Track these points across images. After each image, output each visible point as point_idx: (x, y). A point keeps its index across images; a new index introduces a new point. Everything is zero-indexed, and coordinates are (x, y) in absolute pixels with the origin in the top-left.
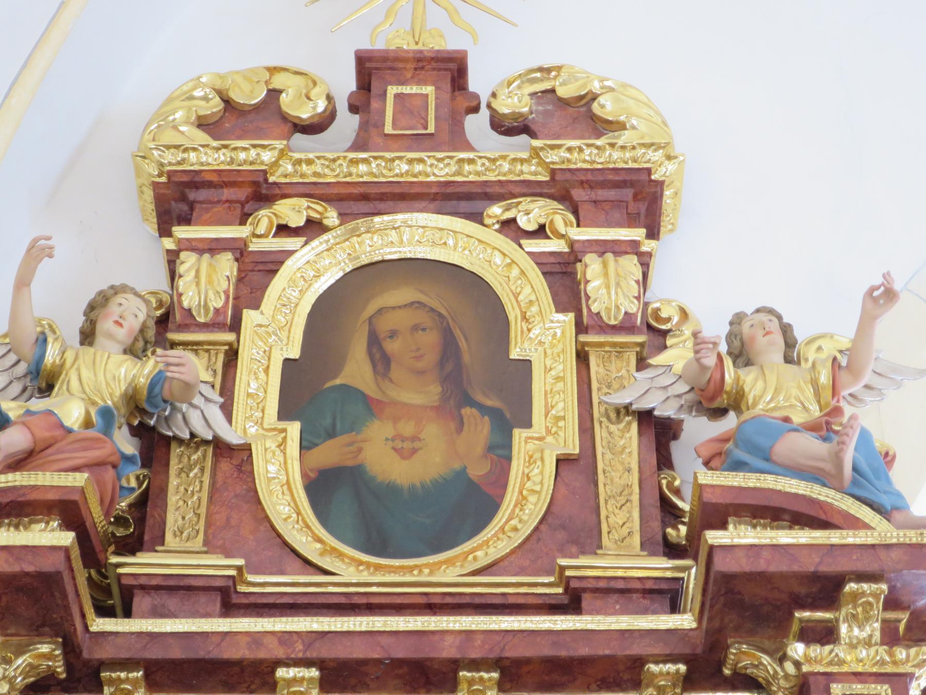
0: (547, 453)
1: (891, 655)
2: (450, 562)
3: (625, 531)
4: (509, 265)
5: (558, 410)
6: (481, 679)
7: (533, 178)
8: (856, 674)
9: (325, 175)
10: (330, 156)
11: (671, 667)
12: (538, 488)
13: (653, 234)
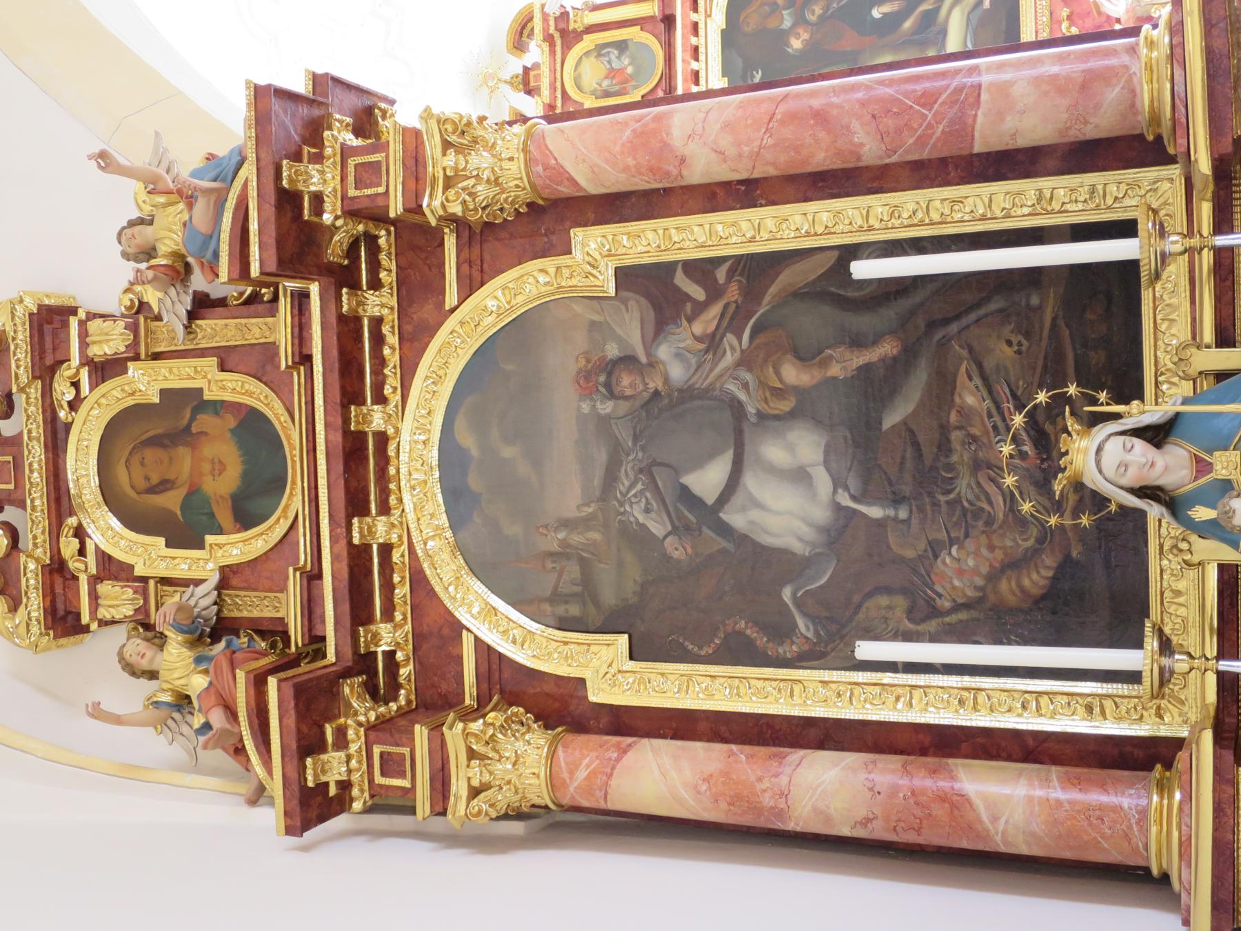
0: (217, 378)
1: (330, 158)
2: (289, 438)
3: (264, 327)
4: (99, 405)
5: (191, 371)
6: (355, 416)
7: (40, 391)
8: (342, 180)
9: (44, 527)
10: (30, 524)
11: (345, 298)
12: (240, 383)
13: (73, 311)
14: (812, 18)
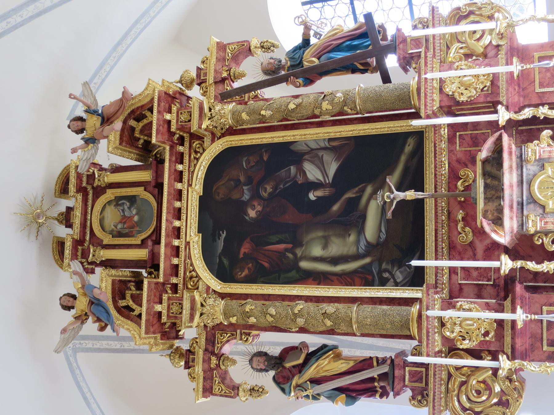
14: (265, 195)
